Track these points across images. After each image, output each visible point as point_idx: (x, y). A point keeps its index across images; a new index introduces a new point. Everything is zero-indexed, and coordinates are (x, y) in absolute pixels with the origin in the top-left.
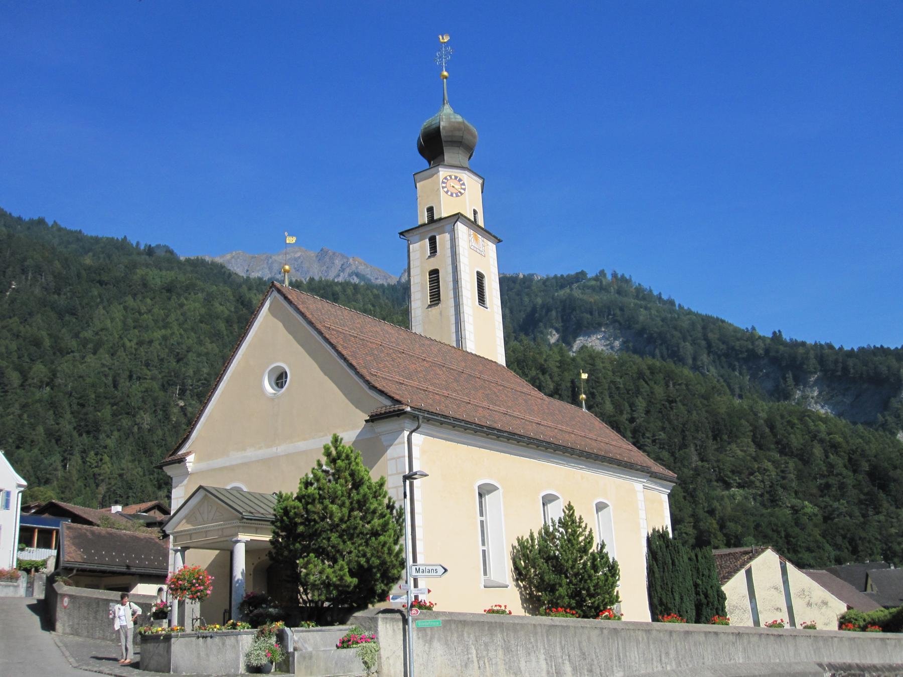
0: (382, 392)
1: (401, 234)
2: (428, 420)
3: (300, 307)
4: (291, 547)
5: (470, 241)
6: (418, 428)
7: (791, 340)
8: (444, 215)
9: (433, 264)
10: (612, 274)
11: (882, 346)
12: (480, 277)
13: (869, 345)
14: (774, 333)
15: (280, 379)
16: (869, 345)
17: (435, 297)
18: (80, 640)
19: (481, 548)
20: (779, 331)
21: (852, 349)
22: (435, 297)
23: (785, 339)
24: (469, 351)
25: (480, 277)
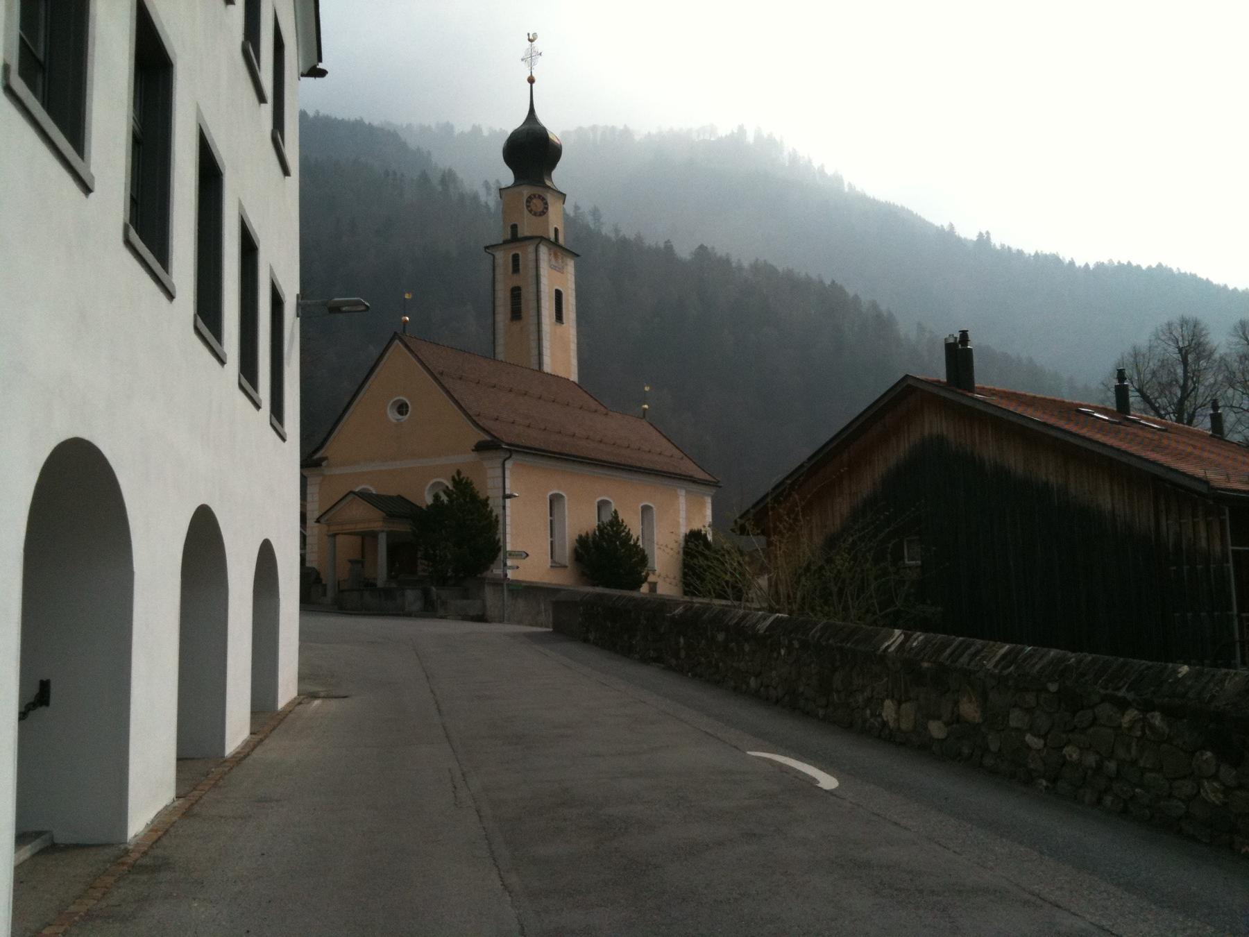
0: (483, 430)
1: (486, 248)
2: (517, 451)
3: (418, 354)
4: (609, 625)
5: (550, 260)
6: (510, 457)
7: (1003, 246)
8: (527, 234)
9: (516, 281)
10: (580, 537)
11: (1129, 263)
12: (559, 295)
13: (1111, 261)
14: (981, 235)
15: (402, 408)
16: (1111, 261)
17: (516, 314)
18: (681, 608)
19: (549, 518)
20: (988, 233)
21: (1087, 265)
22: (516, 314)
23: (995, 245)
24: (546, 372)
25: (559, 295)
